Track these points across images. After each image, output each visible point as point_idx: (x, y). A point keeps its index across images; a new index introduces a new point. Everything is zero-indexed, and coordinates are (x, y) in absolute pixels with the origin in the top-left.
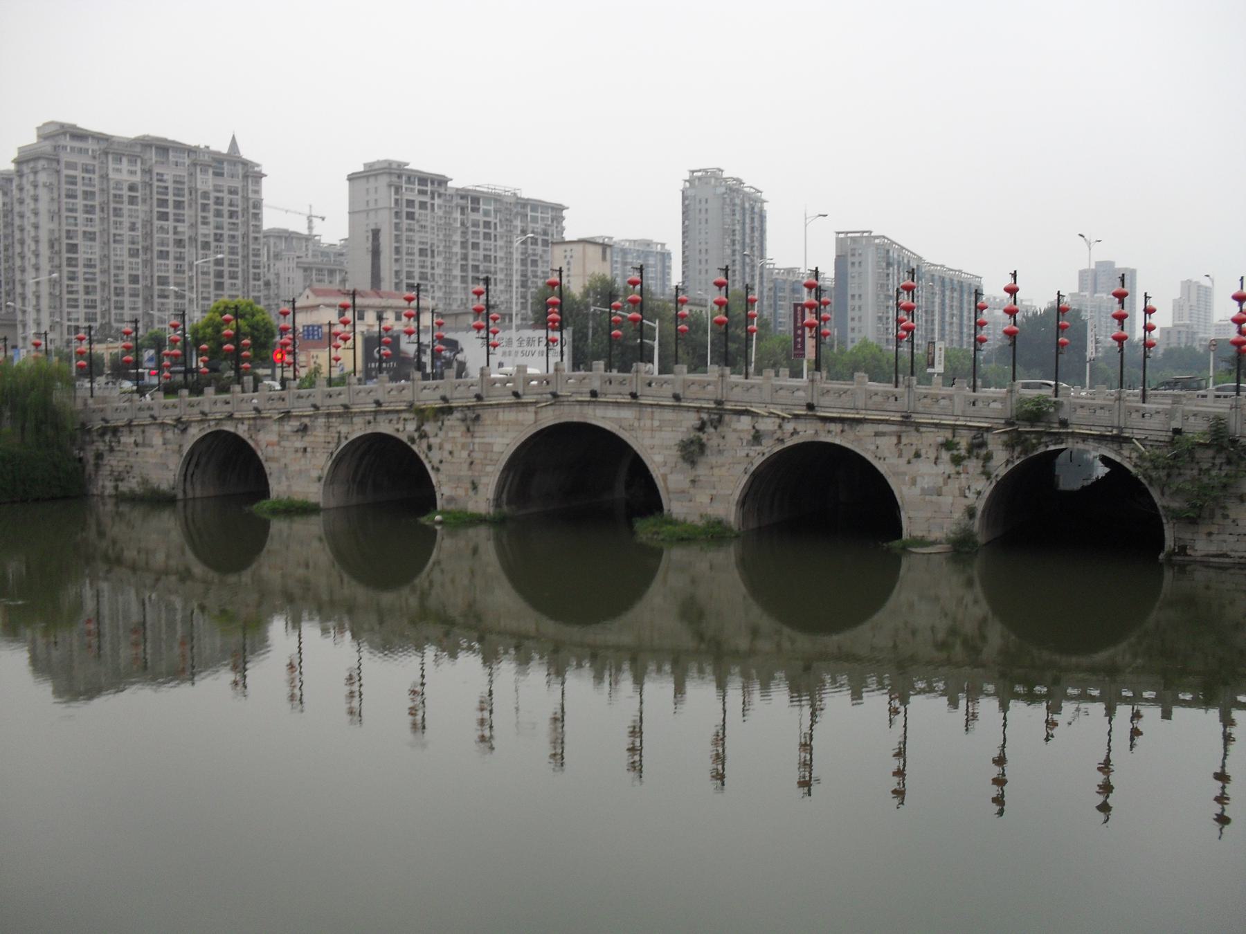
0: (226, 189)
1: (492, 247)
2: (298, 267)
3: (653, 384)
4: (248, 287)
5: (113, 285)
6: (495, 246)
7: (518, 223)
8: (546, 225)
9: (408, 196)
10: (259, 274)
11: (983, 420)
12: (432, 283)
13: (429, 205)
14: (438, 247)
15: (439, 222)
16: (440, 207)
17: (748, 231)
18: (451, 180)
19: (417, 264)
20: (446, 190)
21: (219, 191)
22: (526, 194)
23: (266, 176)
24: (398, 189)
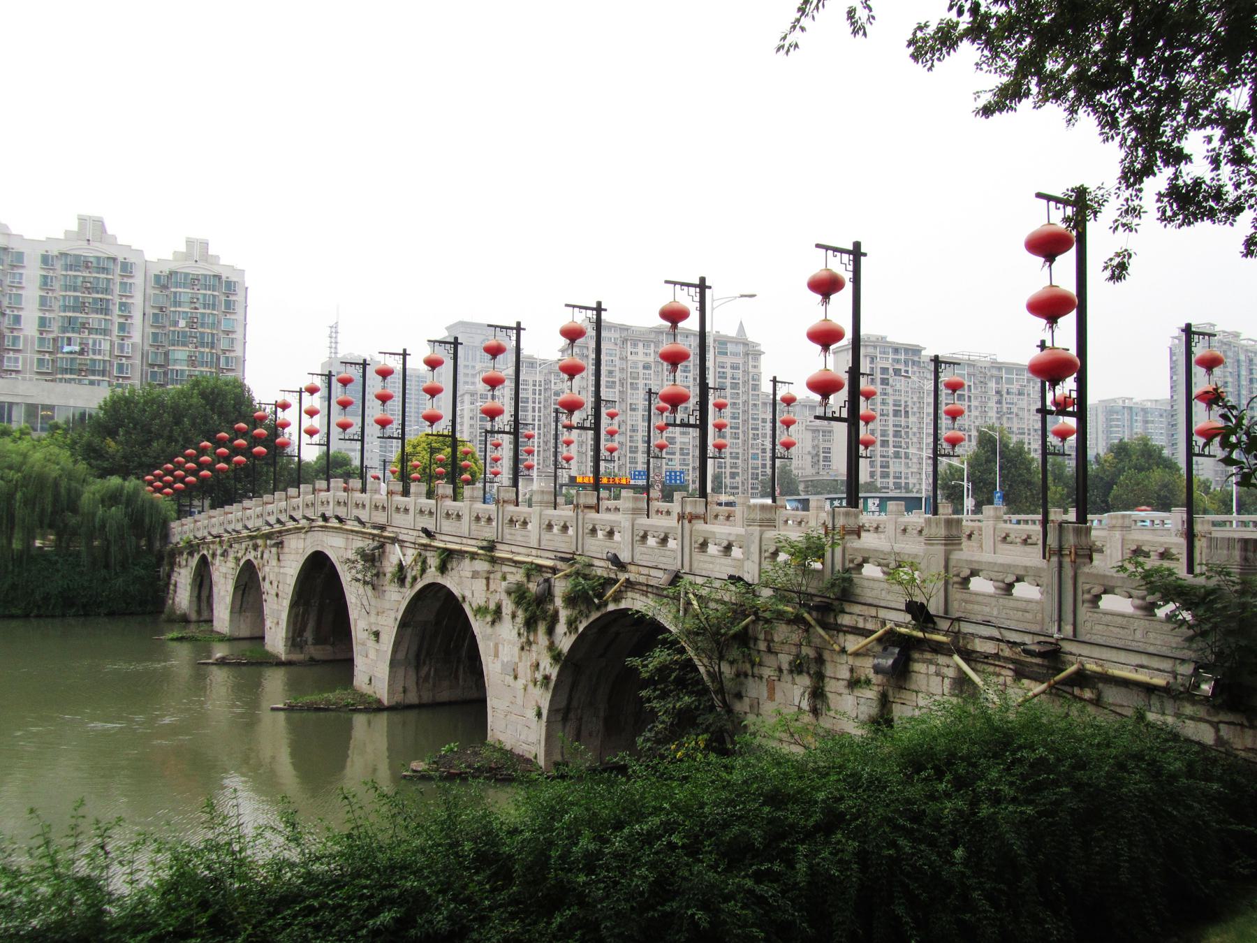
0: (729, 365)
3: (790, 522)
5: (628, 444)
6: (969, 406)
7: (992, 385)
8: (1021, 386)
17: (1244, 382)
19: (891, 423)
21: (723, 367)
22: (1002, 358)
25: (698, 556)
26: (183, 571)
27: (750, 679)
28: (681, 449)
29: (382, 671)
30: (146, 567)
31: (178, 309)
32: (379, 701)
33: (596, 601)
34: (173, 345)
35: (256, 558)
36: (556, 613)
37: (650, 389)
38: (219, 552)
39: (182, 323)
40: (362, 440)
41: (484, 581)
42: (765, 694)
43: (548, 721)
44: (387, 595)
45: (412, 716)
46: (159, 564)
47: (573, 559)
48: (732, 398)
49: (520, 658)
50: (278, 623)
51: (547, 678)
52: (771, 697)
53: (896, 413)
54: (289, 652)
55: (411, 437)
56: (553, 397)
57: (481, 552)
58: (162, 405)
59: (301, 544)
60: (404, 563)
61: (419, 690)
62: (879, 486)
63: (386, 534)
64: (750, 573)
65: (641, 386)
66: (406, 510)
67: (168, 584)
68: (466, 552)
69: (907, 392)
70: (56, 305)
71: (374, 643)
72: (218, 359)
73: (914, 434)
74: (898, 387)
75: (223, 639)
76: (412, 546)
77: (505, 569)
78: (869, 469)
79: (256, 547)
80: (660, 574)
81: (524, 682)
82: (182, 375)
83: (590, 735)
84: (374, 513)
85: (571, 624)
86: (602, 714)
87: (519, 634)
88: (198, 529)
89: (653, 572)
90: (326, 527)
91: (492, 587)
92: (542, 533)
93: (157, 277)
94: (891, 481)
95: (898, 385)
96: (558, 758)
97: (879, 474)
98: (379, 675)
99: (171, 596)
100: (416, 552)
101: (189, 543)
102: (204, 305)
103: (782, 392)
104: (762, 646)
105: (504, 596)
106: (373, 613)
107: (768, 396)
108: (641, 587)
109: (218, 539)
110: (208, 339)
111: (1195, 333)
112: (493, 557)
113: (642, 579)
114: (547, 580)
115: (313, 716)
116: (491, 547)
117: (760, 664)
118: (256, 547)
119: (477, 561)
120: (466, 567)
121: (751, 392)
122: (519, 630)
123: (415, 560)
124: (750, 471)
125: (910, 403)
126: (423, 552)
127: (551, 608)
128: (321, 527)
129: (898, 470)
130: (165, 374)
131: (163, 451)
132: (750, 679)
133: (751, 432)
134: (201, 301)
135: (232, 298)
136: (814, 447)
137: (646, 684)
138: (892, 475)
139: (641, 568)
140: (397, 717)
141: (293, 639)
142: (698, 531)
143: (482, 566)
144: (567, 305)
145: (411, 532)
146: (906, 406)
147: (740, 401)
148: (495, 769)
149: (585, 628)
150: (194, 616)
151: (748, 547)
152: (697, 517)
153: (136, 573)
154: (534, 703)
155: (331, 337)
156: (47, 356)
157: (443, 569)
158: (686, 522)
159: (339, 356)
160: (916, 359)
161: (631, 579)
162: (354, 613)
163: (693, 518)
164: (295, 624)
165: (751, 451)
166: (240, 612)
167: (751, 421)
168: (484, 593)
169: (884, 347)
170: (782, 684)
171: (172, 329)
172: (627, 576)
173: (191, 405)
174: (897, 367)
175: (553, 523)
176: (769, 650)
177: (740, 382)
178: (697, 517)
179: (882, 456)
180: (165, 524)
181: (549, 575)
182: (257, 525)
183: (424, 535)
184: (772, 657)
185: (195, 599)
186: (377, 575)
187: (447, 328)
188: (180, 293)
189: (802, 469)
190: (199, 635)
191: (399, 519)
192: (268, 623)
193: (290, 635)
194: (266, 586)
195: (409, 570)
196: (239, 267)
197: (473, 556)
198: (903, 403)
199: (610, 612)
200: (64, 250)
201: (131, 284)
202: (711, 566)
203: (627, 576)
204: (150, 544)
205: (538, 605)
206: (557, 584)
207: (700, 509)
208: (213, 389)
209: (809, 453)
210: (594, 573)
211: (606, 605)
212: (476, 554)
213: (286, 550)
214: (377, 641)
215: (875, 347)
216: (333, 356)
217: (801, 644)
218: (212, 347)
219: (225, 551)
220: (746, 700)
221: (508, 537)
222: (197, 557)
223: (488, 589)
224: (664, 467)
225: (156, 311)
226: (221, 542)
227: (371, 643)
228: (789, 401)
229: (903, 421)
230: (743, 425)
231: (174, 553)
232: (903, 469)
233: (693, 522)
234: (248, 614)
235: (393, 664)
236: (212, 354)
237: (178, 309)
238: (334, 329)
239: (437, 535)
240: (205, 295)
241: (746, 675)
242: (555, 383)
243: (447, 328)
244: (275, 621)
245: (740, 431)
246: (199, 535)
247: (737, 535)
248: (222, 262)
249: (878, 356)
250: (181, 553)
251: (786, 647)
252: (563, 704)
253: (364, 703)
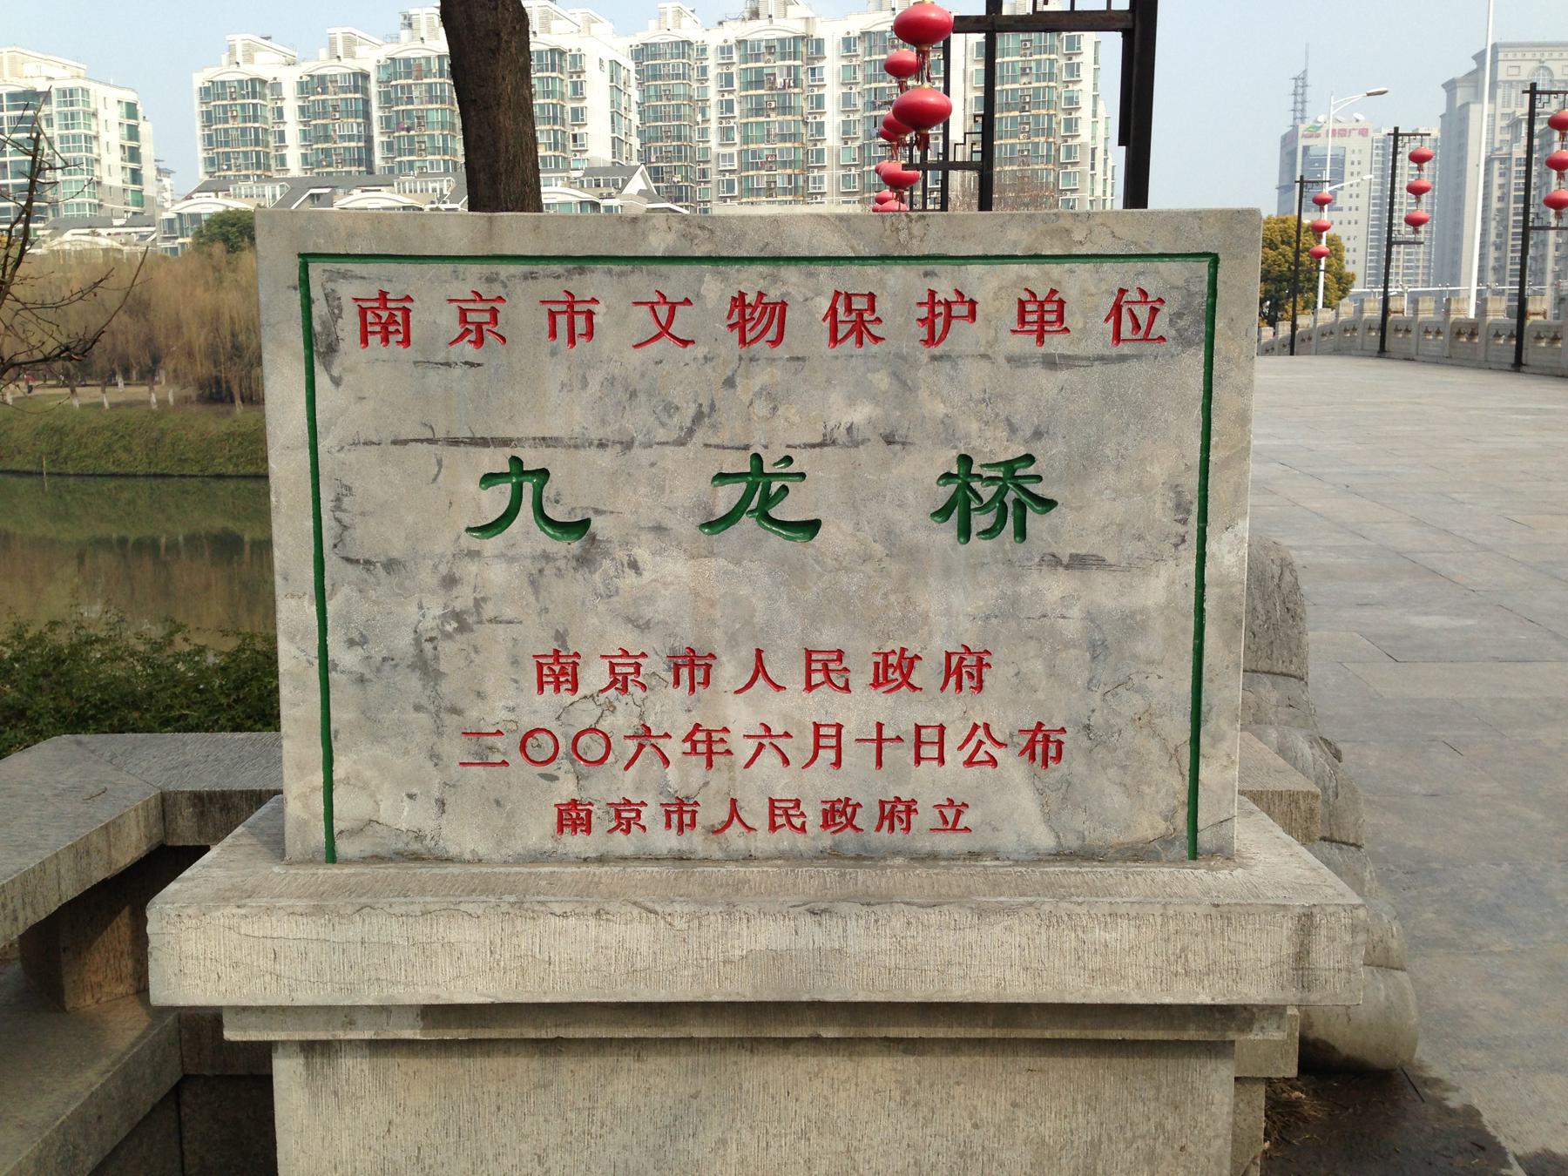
70: (860, 103)
111: (1403, 135)
155: (1295, 94)
156: (853, 171)
200: (866, 28)
201: (1078, 64)
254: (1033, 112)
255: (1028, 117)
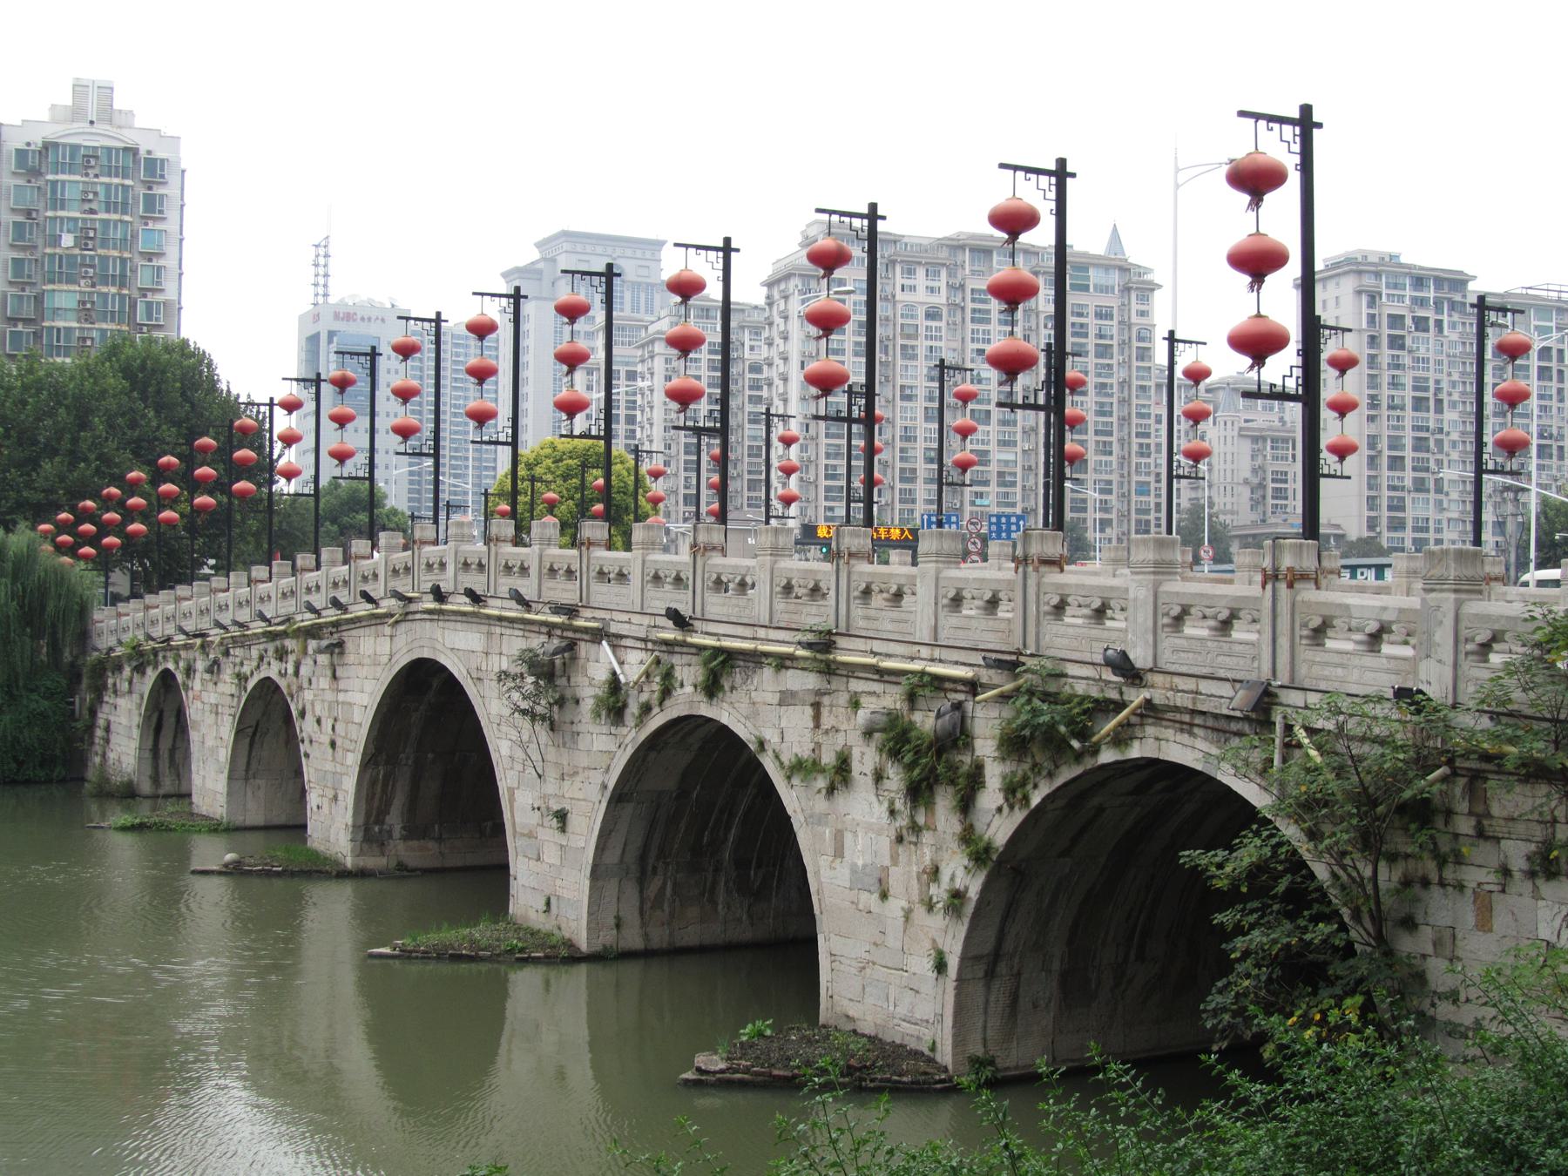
0: (1091, 311)
1: (1554, 392)
2: (1240, 436)
4: (1129, 467)
5: (898, 465)
9: (1388, 308)
10: (1148, 446)
11: (740, 631)
12: (1439, 457)
13: (1431, 323)
14: (1450, 394)
15: (1452, 352)
16: (1453, 326)
18: (1474, 278)
19: (1408, 423)
20: (1464, 296)
21: (1080, 315)
23: (1160, 286)
24: (1373, 298)
25: (1306, 653)
26: (123, 702)
27: (1436, 891)
28: (1001, 474)
29: (575, 889)
30: (50, 695)
31: (61, 213)
32: (569, 944)
33: (1076, 744)
34: (52, 282)
35: (283, 674)
36: (978, 769)
37: (942, 361)
38: (200, 665)
39: (68, 240)
40: (436, 456)
41: (809, 711)
42: (1470, 919)
43: (960, 980)
44: (583, 743)
45: (632, 972)
46: (72, 689)
47: (1016, 664)
48: (1099, 375)
49: (895, 859)
50: (335, 798)
51: (957, 895)
52: (1484, 924)
53: (1419, 404)
54: (359, 853)
55: (530, 444)
56: (748, 375)
57: (801, 652)
58: (58, 394)
59: (384, 646)
60: (622, 679)
61: (644, 924)
62: (1385, 544)
63: (580, 623)
64: (1434, 681)
65: (922, 351)
66: (622, 577)
67: (91, 728)
68: (766, 655)
69: (1440, 363)
71: (557, 833)
72: (133, 306)
73: (1454, 444)
74: (1422, 353)
75: (216, 828)
76: (639, 644)
77: (856, 685)
78: (1367, 513)
79: (281, 655)
80: (1225, 690)
81: (904, 904)
82: (68, 339)
83: (1035, 1006)
84: (548, 583)
85: (1014, 791)
86: (1056, 966)
87: (892, 812)
88: (153, 623)
89: (1206, 687)
90: (441, 612)
91: (827, 721)
92: (942, 614)
93: (21, 154)
94: (1408, 535)
95: (1422, 350)
96: (979, 1051)
97: (1384, 522)
98: (565, 894)
99: (98, 748)
100: (649, 659)
101: (137, 650)
102: (108, 204)
103: (1184, 359)
104: (1465, 826)
105: (854, 740)
106: (552, 775)
107: (1163, 371)
108: (1178, 717)
109: (198, 641)
110: (114, 269)
111: (948, 368)
112: (828, 663)
113: (1182, 700)
114: (958, 706)
115: (447, 969)
116: (824, 643)
117: (1459, 860)
118: (281, 655)
119: (790, 672)
120: (766, 683)
121: (1135, 363)
122: (892, 803)
123: (648, 674)
124: (1134, 516)
125: (1445, 385)
126: (664, 657)
127: (967, 759)
128: (430, 612)
129: (1422, 514)
130: (37, 336)
131: (62, 479)
132: (1436, 891)
133: (1135, 441)
134: (102, 197)
135: (158, 190)
136: (1254, 471)
137: (1229, 898)
138: (1409, 524)
139: (1176, 680)
140: (605, 974)
141: (367, 830)
142: (1308, 604)
143: (802, 681)
144: (1003, 166)
145: (636, 619)
146: (1438, 390)
147: (1114, 381)
148: (860, 1069)
149: (1044, 800)
150: (146, 787)
151: (1429, 634)
152: (1304, 577)
153: (33, 706)
154: (927, 945)
155: (316, 265)
157: (712, 688)
158: (1282, 586)
159: (332, 300)
160: (1458, 297)
161: (1156, 701)
162: (506, 779)
163: (1295, 578)
164: (370, 798)
165: (1135, 478)
166: (246, 779)
167: (1135, 421)
168: (808, 735)
169: (1396, 275)
170: (1510, 899)
171: (48, 250)
172: (1145, 694)
173: (104, 392)
174: (1421, 313)
175: (966, 594)
176: (1481, 834)
177: (1115, 342)
178: (1304, 577)
179: (1392, 488)
180: (83, 612)
181: (961, 697)
182: (282, 611)
183: (670, 624)
184: (1486, 847)
185: (147, 755)
186: (561, 702)
187: (539, 245)
188: (63, 182)
189: (1232, 513)
190: (174, 821)
191: (603, 594)
192: (313, 799)
193: (361, 821)
194: (306, 728)
195: (634, 693)
196: (169, 131)
197: (783, 662)
198: (1431, 384)
199: (1104, 766)
201: (162, 196)
202: (1340, 671)
203: (1145, 694)
204: (55, 649)
205: (939, 754)
206: (979, 713)
207: (1309, 563)
208: (144, 362)
209: (1246, 482)
210: (1067, 689)
211: (1095, 751)
212: (791, 657)
213: (350, 658)
214: (563, 829)
215: (1378, 275)
216: (321, 300)
217: (1555, 821)
218: (122, 285)
219: (216, 662)
220: (1426, 934)
221: (859, 624)
222: (151, 675)
223: (817, 726)
224: (968, 508)
225: (20, 219)
226: (204, 647)
227: (549, 835)
228: (1197, 375)
229: (1431, 418)
230: (1121, 426)
231: (107, 666)
232: (1432, 513)
233: (1297, 586)
234: (261, 782)
235: (597, 873)
236: (122, 297)
237: (61, 213)
238: (322, 254)
239: (697, 624)
240: (108, 186)
241: (1426, 883)
242: (752, 348)
243: (539, 245)
244: (330, 794)
245: (1114, 439)
246: (157, 632)
247: (1401, 611)
248: (138, 123)
249: (1384, 291)
250: (119, 668)
251: (1520, 828)
252: (988, 947)
253: (542, 946)
254: (100, 251)
255: (92, 257)
